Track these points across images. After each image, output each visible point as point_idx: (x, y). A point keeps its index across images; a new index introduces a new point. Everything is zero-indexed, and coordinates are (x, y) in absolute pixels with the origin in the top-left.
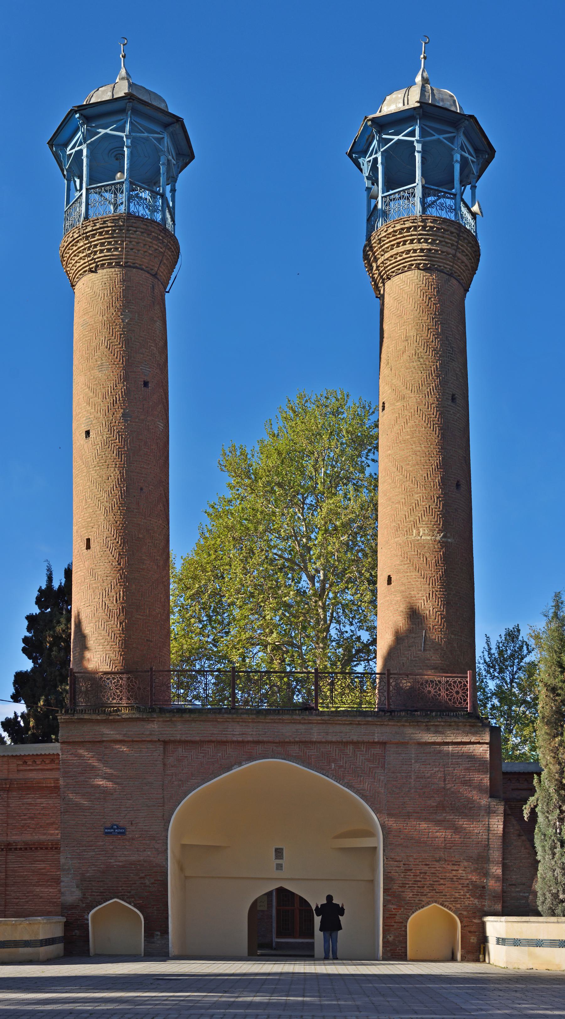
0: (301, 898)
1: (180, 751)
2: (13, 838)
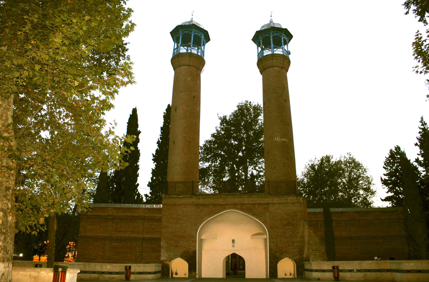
0: (239, 256)
2: (145, 236)
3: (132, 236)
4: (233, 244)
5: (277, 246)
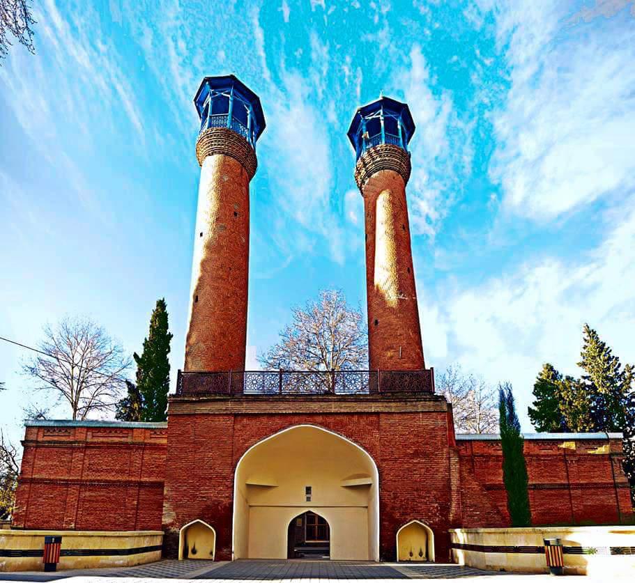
0: (319, 516)
1: (245, 421)
3: (120, 478)
4: (308, 496)
5: (395, 498)
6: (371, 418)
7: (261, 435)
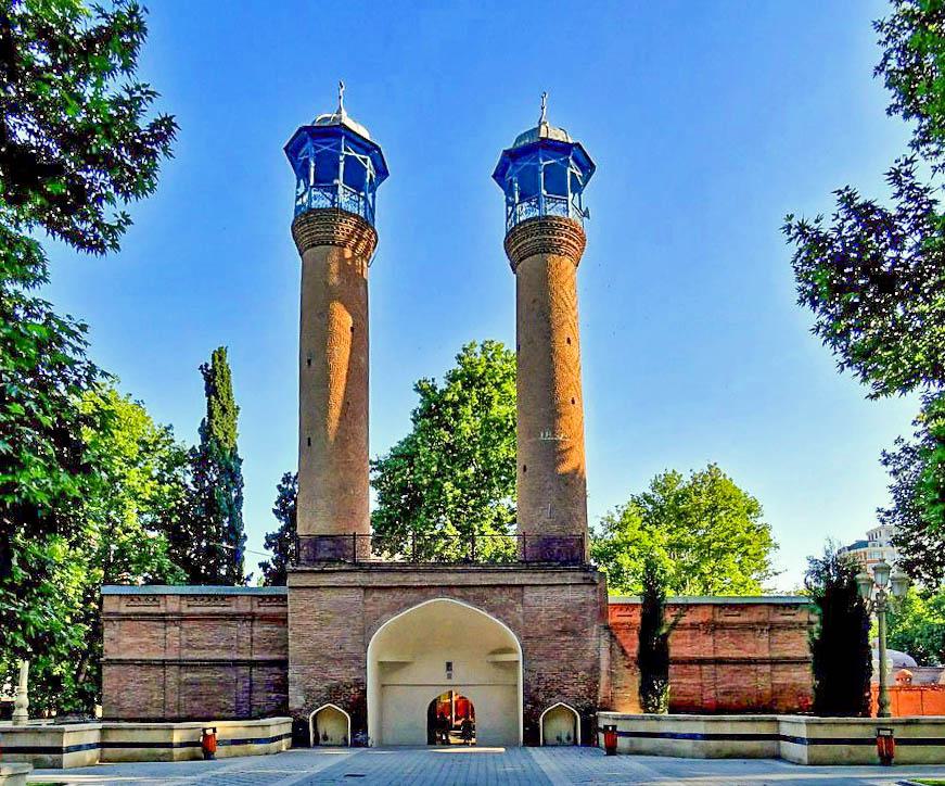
1: (376, 595)
6: (514, 591)
7: (396, 609)
